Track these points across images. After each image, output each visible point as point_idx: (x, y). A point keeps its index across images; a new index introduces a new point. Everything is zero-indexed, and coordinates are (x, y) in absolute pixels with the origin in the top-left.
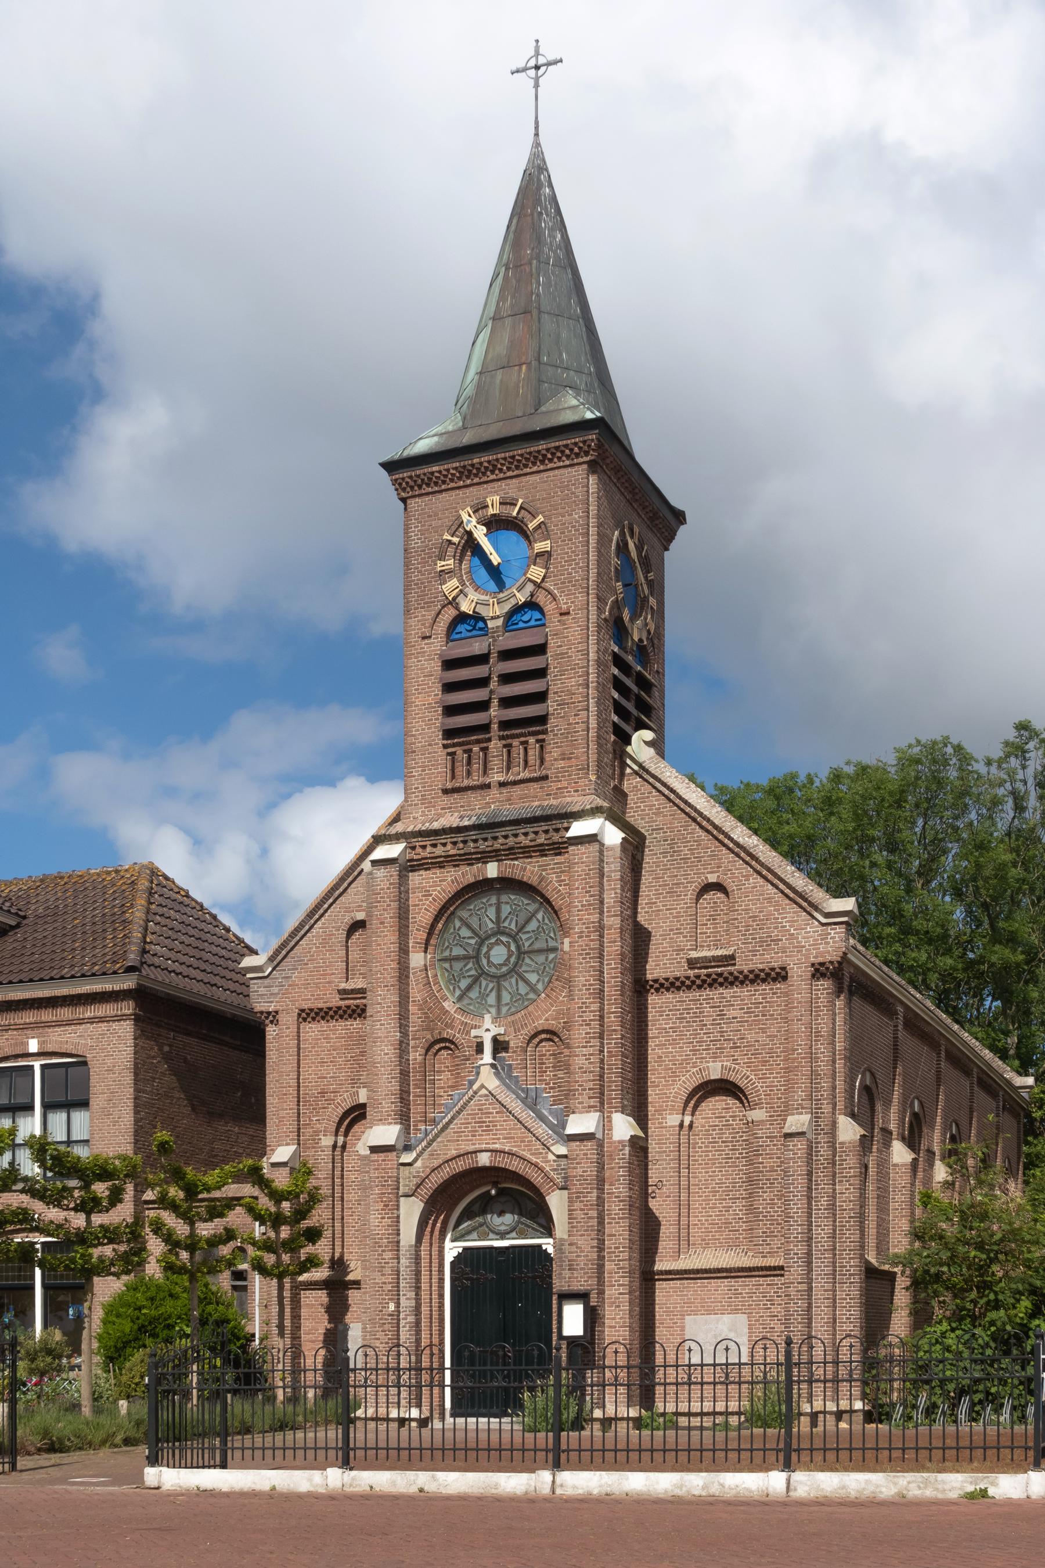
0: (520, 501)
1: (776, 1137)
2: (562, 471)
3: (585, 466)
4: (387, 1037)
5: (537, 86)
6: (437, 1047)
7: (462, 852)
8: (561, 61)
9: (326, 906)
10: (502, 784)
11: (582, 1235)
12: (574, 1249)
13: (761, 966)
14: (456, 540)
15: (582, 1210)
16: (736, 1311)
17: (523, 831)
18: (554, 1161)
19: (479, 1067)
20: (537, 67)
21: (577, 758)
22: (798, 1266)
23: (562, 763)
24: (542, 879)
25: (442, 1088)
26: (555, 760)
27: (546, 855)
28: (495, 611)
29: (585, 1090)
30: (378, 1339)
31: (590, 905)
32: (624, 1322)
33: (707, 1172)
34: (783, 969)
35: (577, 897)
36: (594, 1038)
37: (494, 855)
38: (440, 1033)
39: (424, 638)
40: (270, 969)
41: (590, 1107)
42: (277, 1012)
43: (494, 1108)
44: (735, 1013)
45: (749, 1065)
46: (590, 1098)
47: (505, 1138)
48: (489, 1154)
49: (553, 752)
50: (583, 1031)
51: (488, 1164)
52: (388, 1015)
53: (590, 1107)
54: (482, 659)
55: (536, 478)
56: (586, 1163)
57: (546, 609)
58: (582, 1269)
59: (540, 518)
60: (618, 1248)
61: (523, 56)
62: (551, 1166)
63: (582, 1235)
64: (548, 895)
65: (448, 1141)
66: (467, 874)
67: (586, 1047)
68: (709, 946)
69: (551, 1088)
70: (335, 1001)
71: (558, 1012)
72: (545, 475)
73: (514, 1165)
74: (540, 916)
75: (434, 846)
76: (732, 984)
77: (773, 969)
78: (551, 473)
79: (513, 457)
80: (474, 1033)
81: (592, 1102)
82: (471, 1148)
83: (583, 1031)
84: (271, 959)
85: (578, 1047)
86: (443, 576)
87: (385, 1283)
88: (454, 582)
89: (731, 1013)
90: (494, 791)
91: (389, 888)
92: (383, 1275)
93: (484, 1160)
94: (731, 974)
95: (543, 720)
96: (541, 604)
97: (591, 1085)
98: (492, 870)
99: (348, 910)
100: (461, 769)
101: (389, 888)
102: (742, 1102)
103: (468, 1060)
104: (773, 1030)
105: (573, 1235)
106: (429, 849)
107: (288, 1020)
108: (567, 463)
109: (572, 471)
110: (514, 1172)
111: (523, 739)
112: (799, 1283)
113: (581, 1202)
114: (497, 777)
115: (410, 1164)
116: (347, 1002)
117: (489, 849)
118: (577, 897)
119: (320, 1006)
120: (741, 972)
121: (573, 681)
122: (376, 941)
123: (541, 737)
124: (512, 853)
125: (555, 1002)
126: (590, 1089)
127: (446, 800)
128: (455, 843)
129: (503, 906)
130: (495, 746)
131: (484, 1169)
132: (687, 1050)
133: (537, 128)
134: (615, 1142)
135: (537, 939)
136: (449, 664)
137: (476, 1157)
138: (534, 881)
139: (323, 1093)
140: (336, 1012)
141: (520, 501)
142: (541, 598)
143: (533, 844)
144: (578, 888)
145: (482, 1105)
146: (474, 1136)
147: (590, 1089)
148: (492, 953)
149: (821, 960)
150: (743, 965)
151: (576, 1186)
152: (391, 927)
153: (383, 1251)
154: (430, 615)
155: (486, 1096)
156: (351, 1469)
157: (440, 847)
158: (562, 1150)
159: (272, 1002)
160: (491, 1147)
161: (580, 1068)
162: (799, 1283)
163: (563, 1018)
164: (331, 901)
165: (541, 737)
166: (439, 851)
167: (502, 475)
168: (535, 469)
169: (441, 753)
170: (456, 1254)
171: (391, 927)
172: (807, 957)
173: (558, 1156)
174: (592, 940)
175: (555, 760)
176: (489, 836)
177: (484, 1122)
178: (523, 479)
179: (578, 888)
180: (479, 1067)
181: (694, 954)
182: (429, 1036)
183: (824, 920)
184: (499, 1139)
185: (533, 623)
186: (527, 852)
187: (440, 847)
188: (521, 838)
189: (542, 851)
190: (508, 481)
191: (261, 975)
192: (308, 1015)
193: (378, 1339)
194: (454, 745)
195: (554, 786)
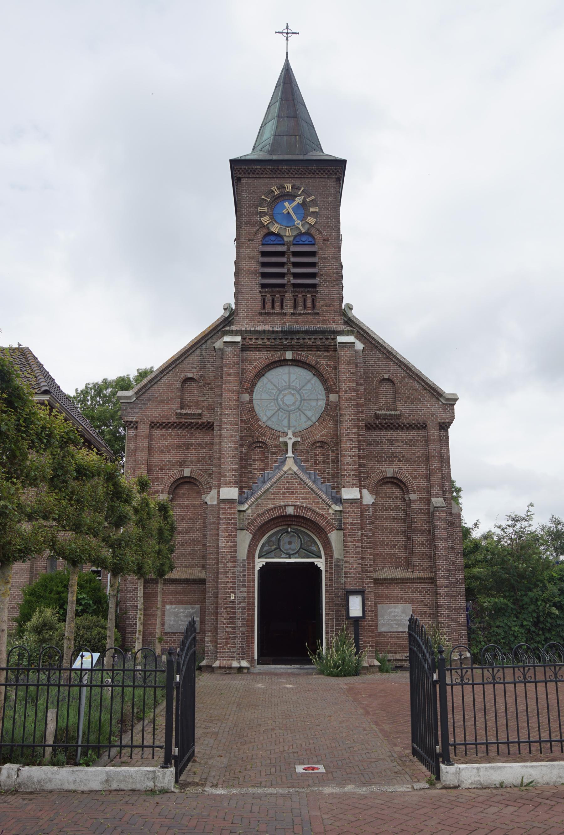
0: (302, 188)
1: (423, 509)
2: (323, 180)
3: (335, 180)
4: (231, 437)
5: (287, 39)
6: (254, 446)
7: (273, 344)
8: (298, 33)
9: (171, 368)
10: (292, 314)
11: (352, 557)
12: (347, 565)
13: (413, 421)
14: (268, 200)
15: (352, 542)
16: (405, 602)
17: (309, 337)
18: (333, 514)
19: (286, 458)
20: (287, 33)
21: (334, 307)
22: (444, 578)
23: (325, 308)
24: (317, 363)
25: (256, 469)
26: (322, 306)
27: (320, 351)
28: (289, 234)
29: (350, 475)
30: (223, 617)
31: (350, 378)
32: (372, 608)
33: (383, 526)
34: (424, 423)
35: (343, 373)
36: (355, 447)
37: (291, 348)
38: (257, 438)
39: (249, 240)
40: (135, 399)
41: (353, 485)
42: (137, 422)
43: (297, 482)
44: (399, 444)
45: (407, 470)
46: (353, 480)
47: (303, 499)
48: (293, 508)
49: (320, 303)
50: (349, 443)
51: (292, 514)
52: (231, 425)
53: (353, 485)
54: (282, 254)
55: (310, 180)
56: (354, 516)
57: (316, 237)
58: (352, 577)
59: (313, 197)
60: (367, 565)
61: (282, 28)
62: (330, 516)
63: (352, 557)
64: (321, 371)
65: (268, 499)
66: (276, 356)
67: (350, 452)
68: (384, 409)
69: (322, 473)
70: (173, 419)
71: (328, 432)
72: (315, 180)
73: (309, 515)
74: (313, 382)
75: (257, 339)
76: (397, 429)
77: (419, 423)
78: (317, 180)
79: (299, 169)
80: (281, 439)
81: (354, 482)
82: (283, 504)
83: (349, 443)
84: (136, 393)
85: (346, 451)
86: (263, 214)
87: (228, 582)
88: (267, 218)
89: (398, 444)
90: (288, 317)
91: (233, 357)
92: (227, 577)
93: (290, 511)
94: (397, 423)
95: (314, 286)
96: (313, 234)
97: (354, 472)
98: (289, 355)
99: (183, 372)
100: (269, 304)
101: (233, 357)
102: (401, 488)
103: (275, 454)
104: (419, 454)
105: (347, 557)
106: (254, 341)
107: (144, 427)
108: (326, 176)
109: (328, 181)
110: (309, 519)
111: (304, 294)
112: (445, 587)
113: (351, 538)
114: (290, 310)
115: (244, 511)
116: (180, 420)
117: (289, 344)
118: (343, 373)
119: (164, 421)
120: (403, 423)
121: (331, 271)
122: (225, 384)
123: (314, 294)
124: (301, 347)
125: (326, 427)
126: (353, 475)
127: (260, 318)
128: (268, 339)
129: (292, 375)
130: (288, 296)
131: (290, 516)
132: (374, 460)
133: (287, 55)
134: (364, 505)
135: (311, 393)
136: (264, 254)
137: (285, 509)
138: (313, 363)
139: (162, 469)
140: (172, 425)
141: (302, 188)
142: (313, 232)
143: (314, 344)
144: (344, 368)
145: (289, 479)
146: (284, 497)
147: (353, 475)
148: (285, 398)
149: (443, 421)
150: (405, 420)
151: (349, 529)
152: (235, 378)
153: (227, 562)
154: (253, 231)
155: (292, 474)
156: (453, 765)
157: (260, 340)
158: (338, 508)
159: (134, 417)
160: (295, 503)
161: (347, 463)
162: (445, 587)
163: (330, 436)
164: (174, 366)
165: (314, 294)
166: (260, 342)
167: (292, 176)
168: (309, 176)
169: (258, 297)
170: (261, 566)
171: (235, 378)
172: (437, 419)
173: (336, 511)
174: (353, 396)
175: (322, 306)
176: (289, 338)
177: (291, 489)
178: (303, 180)
179: (344, 368)
180: (286, 458)
181: (378, 412)
182: (251, 440)
183: (445, 402)
184: (299, 499)
185: (307, 243)
186: (310, 348)
187: (260, 340)
188: (307, 341)
189: (318, 349)
190: (295, 179)
191: (129, 401)
192: (154, 425)
193: (223, 617)
194: (266, 292)
195: (321, 318)
